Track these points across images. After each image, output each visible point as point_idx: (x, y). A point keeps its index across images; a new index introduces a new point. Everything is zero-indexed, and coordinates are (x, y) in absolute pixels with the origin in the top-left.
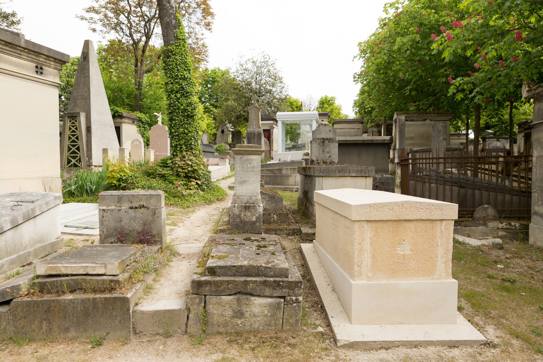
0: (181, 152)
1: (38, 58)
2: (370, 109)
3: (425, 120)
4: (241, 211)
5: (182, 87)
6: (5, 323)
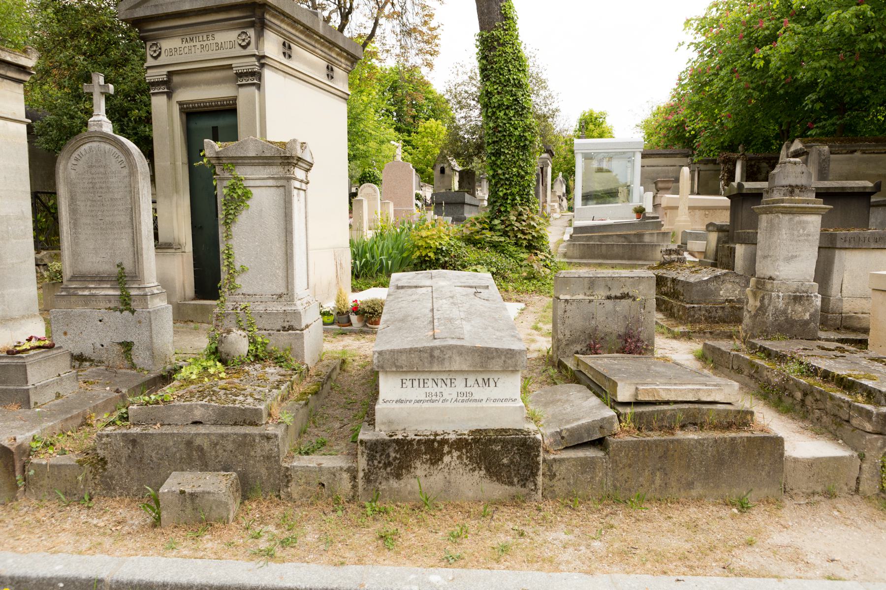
0: (513, 206)
1: (330, 53)
2: (693, 132)
3: (852, 152)
4: (787, 304)
5: (516, 100)
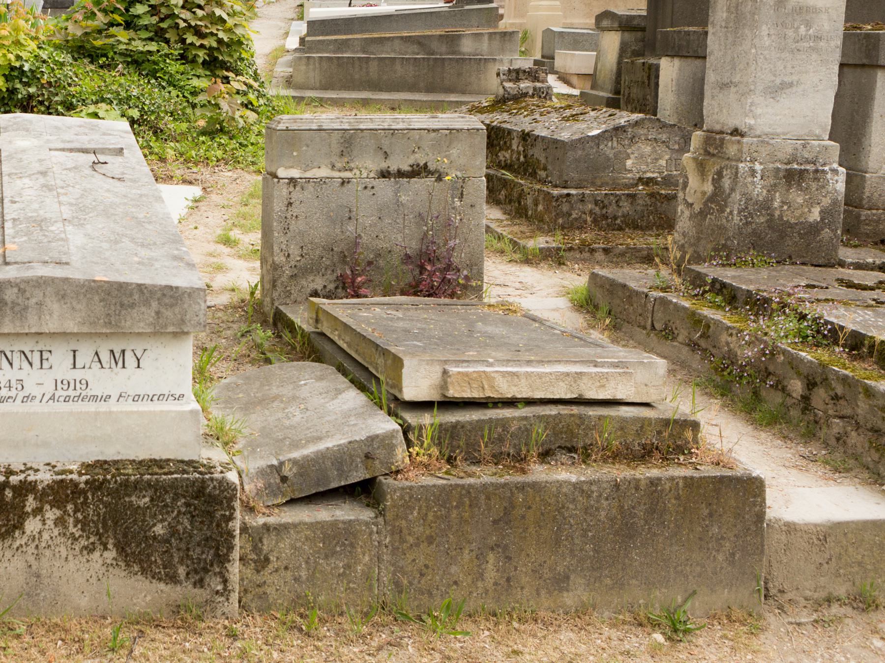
6: (367, 558)
